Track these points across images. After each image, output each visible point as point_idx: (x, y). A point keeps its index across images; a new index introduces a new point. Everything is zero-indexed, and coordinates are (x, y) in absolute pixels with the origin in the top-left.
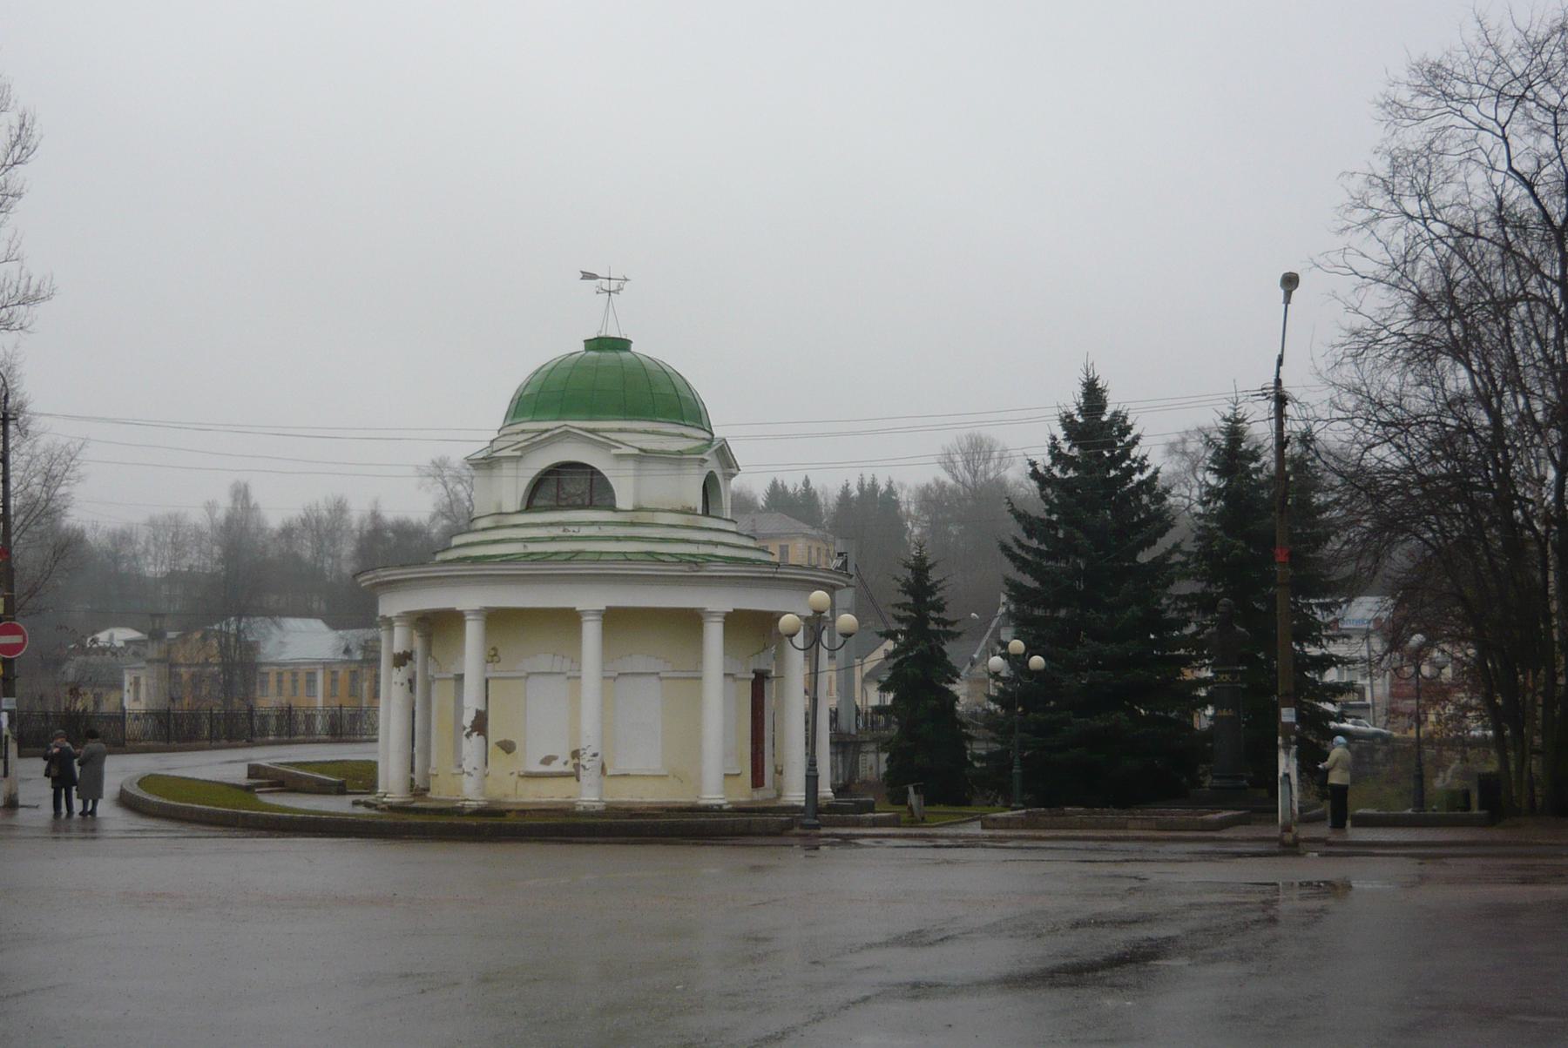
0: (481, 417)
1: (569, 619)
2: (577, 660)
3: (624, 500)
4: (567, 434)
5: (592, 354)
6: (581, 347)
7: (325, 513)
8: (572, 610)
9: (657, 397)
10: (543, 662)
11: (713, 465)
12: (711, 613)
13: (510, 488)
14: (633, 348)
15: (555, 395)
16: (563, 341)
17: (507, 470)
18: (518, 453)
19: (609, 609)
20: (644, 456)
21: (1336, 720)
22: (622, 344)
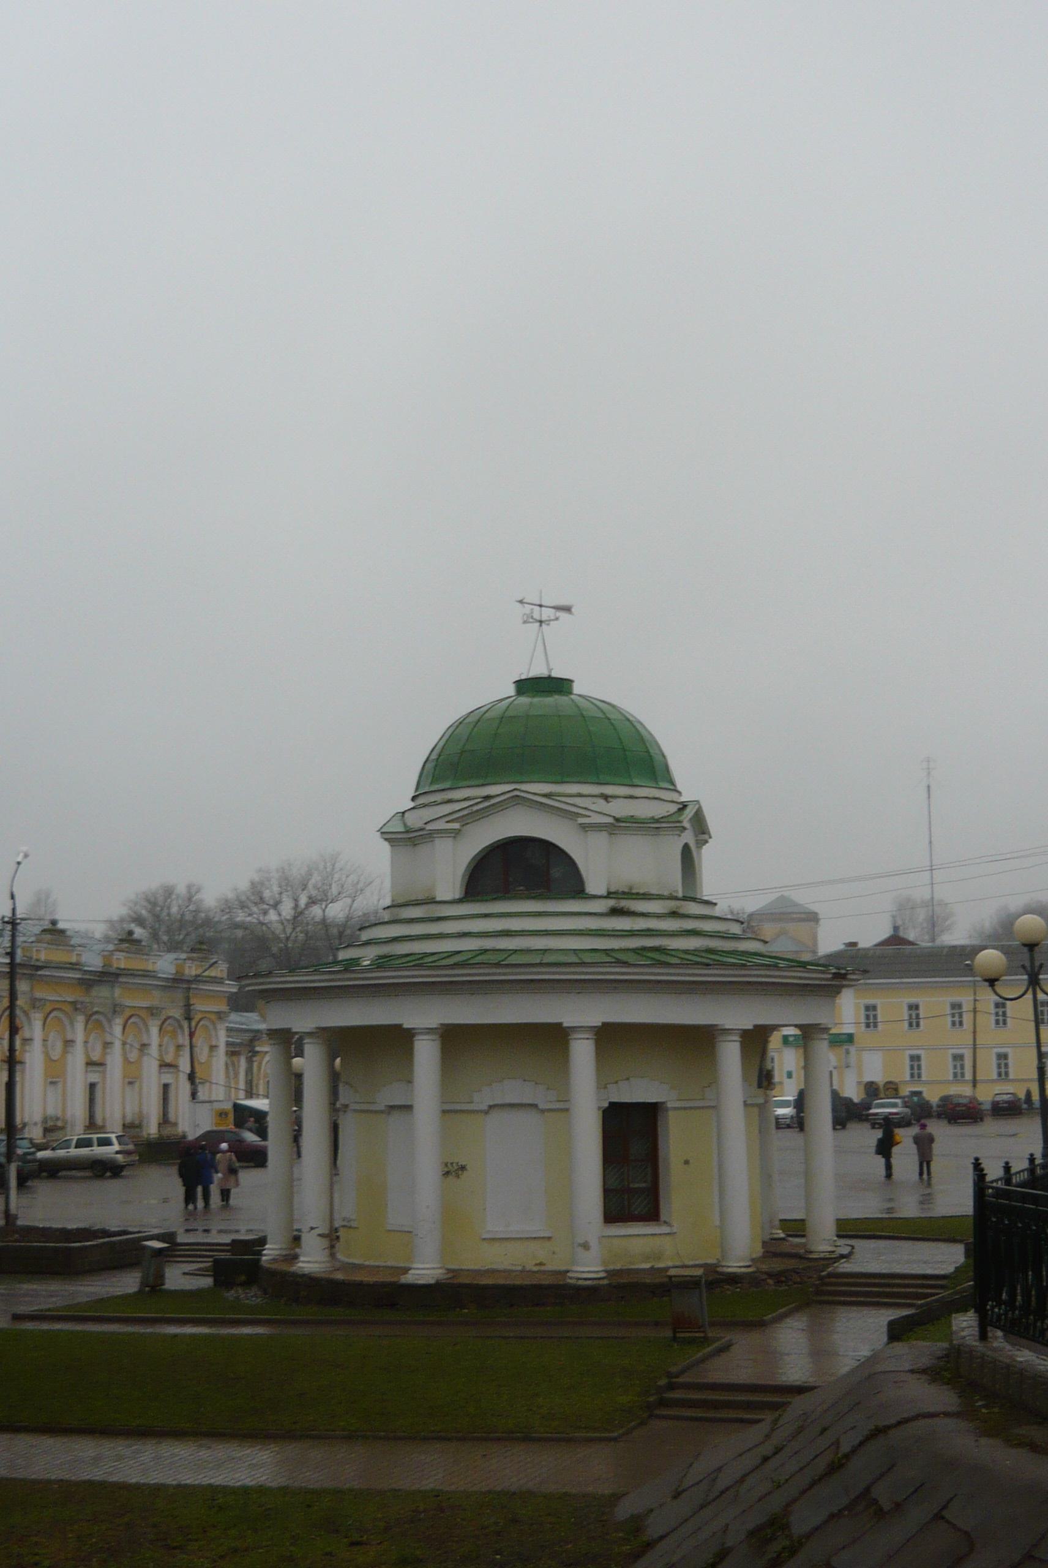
0: (393, 783)
1: (553, 1039)
2: (712, 1080)
3: (595, 884)
4: (517, 800)
5: (524, 700)
6: (511, 690)
7: (174, 910)
8: (398, 1027)
9: (616, 753)
10: (513, 1090)
11: (688, 837)
12: (726, 1031)
13: (447, 867)
14: (577, 689)
15: (472, 757)
16: (491, 686)
17: (443, 847)
18: (456, 826)
19: (605, 1025)
20: (619, 826)
21: (1042, 1281)
22: (558, 686)
